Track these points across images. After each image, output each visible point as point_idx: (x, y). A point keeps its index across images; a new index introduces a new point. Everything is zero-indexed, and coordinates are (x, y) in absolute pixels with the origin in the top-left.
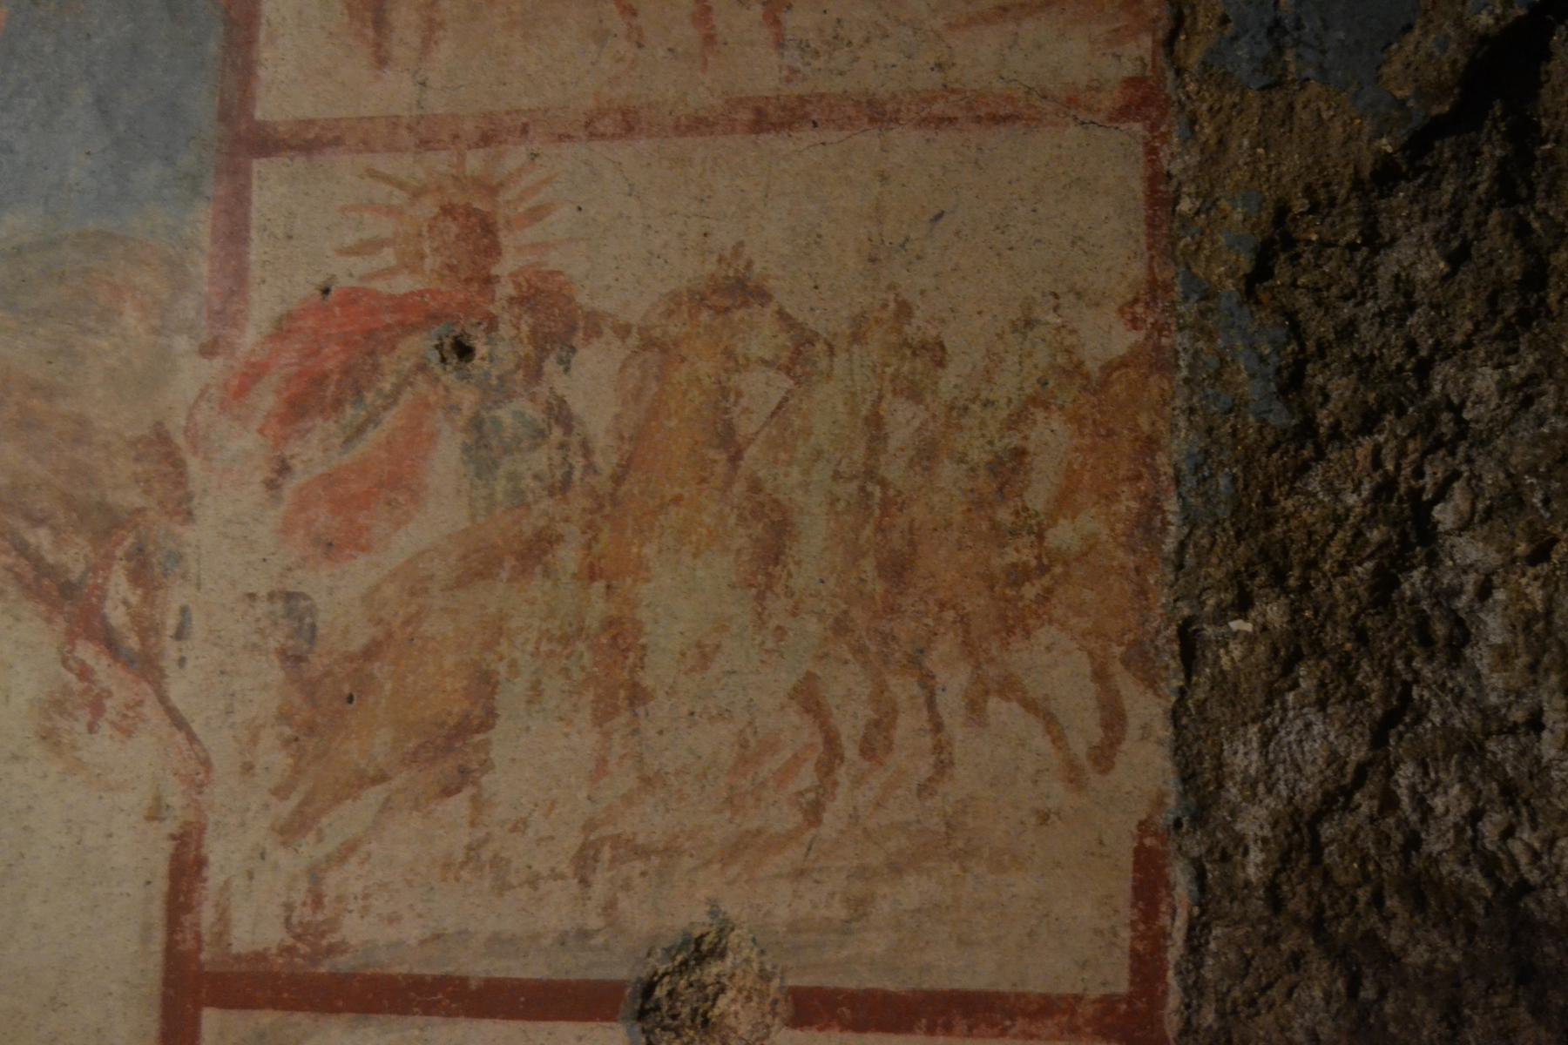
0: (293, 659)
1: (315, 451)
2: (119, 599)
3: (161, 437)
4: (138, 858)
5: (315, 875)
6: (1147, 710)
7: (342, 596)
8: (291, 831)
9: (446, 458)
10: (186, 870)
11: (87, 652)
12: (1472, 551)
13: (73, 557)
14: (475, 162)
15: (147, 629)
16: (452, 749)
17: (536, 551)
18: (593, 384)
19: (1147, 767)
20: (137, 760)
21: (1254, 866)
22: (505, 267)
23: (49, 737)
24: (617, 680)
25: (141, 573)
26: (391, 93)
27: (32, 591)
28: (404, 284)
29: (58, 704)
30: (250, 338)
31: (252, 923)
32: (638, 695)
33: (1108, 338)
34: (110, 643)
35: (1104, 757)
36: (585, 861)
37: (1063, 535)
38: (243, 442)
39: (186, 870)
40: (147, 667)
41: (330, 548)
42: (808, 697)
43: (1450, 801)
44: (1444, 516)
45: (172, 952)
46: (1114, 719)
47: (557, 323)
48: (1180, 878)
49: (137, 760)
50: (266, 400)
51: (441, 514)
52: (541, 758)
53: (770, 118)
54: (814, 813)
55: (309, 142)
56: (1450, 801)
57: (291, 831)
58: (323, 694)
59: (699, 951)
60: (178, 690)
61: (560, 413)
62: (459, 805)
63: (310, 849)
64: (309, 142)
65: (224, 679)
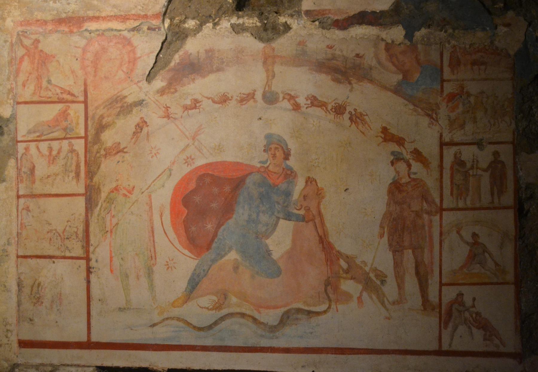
0: (449, 120)
1: (450, 105)
2: (434, 116)
3: (437, 103)
4: (437, 135)
5: (452, 136)
6: (123, 13)
7: (453, 115)
8: (450, 132)
9: (461, 105)
10: (441, 136)
11: (432, 120)
12: (535, 110)
13: (430, 113)
14: (462, 83)
15: (437, 118)
16: (462, 126)
17: (468, 111)
18: (472, 99)
19: (513, 126)
20: (437, 128)
21: (521, 132)
22: (465, 90)
23: (429, 127)
24: (475, 121)
25: (436, 114)
26: (454, 77)
27: (427, 115)
28: (456, 92)
29: (430, 124)
30: (445, 95)
31: (447, 139)
32: (476, 122)
33: (510, 96)
34: (434, 119)
35: (510, 125)
36: (473, 134)
37: (507, 110)
38: (444, 104)
39: (441, 136)
40: (437, 121)
41: (452, 112)
42: (489, 122)
43: (534, 127)
44: (533, 107)
45: (391, 91)
46: (511, 123)
47: (469, 95)
48: (516, 133)
49: (437, 128)
50: (446, 100)
51: (460, 109)
52: (469, 127)
53: (486, 79)
54: (490, 130)
55: (449, 81)
56: (534, 127)
57: (450, 132)
58: (451, 123)
59: (482, 140)
60: (440, 123)
61: (469, 101)
62: (463, 130)
63: (451, 134)
64: (449, 81)
65: (444, 122)
